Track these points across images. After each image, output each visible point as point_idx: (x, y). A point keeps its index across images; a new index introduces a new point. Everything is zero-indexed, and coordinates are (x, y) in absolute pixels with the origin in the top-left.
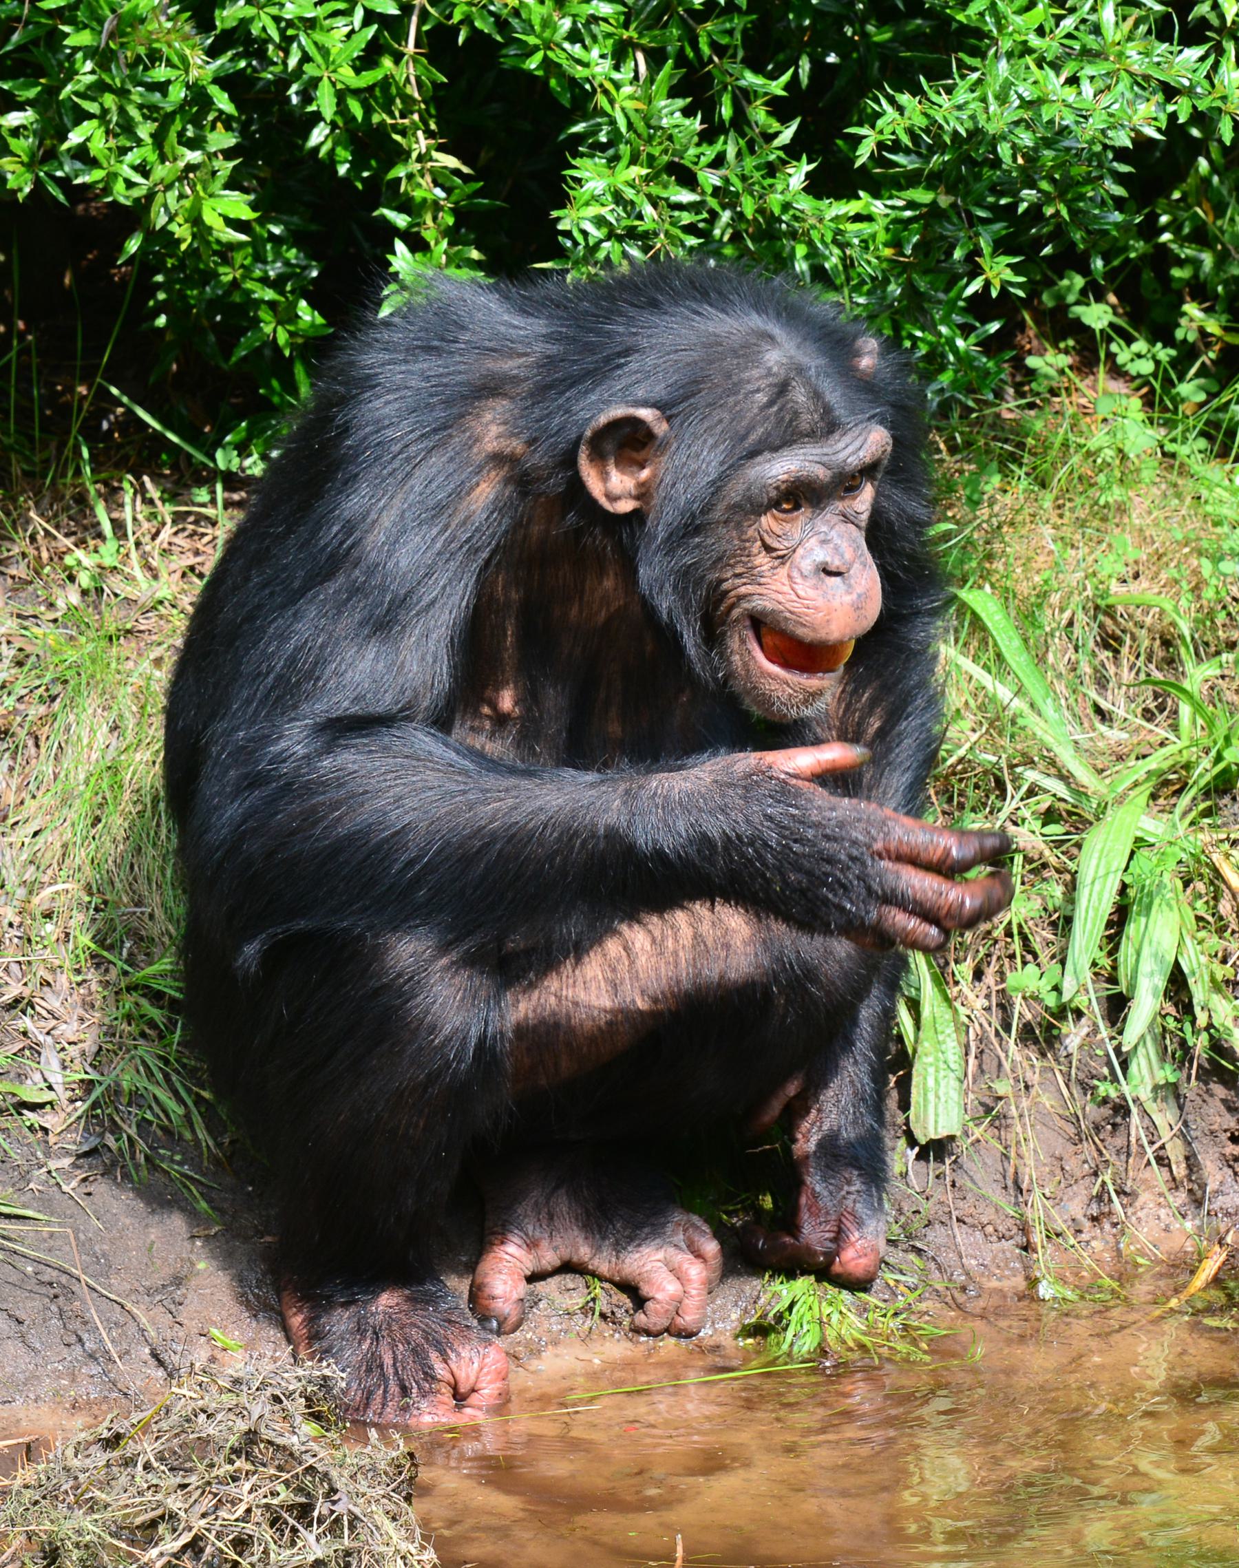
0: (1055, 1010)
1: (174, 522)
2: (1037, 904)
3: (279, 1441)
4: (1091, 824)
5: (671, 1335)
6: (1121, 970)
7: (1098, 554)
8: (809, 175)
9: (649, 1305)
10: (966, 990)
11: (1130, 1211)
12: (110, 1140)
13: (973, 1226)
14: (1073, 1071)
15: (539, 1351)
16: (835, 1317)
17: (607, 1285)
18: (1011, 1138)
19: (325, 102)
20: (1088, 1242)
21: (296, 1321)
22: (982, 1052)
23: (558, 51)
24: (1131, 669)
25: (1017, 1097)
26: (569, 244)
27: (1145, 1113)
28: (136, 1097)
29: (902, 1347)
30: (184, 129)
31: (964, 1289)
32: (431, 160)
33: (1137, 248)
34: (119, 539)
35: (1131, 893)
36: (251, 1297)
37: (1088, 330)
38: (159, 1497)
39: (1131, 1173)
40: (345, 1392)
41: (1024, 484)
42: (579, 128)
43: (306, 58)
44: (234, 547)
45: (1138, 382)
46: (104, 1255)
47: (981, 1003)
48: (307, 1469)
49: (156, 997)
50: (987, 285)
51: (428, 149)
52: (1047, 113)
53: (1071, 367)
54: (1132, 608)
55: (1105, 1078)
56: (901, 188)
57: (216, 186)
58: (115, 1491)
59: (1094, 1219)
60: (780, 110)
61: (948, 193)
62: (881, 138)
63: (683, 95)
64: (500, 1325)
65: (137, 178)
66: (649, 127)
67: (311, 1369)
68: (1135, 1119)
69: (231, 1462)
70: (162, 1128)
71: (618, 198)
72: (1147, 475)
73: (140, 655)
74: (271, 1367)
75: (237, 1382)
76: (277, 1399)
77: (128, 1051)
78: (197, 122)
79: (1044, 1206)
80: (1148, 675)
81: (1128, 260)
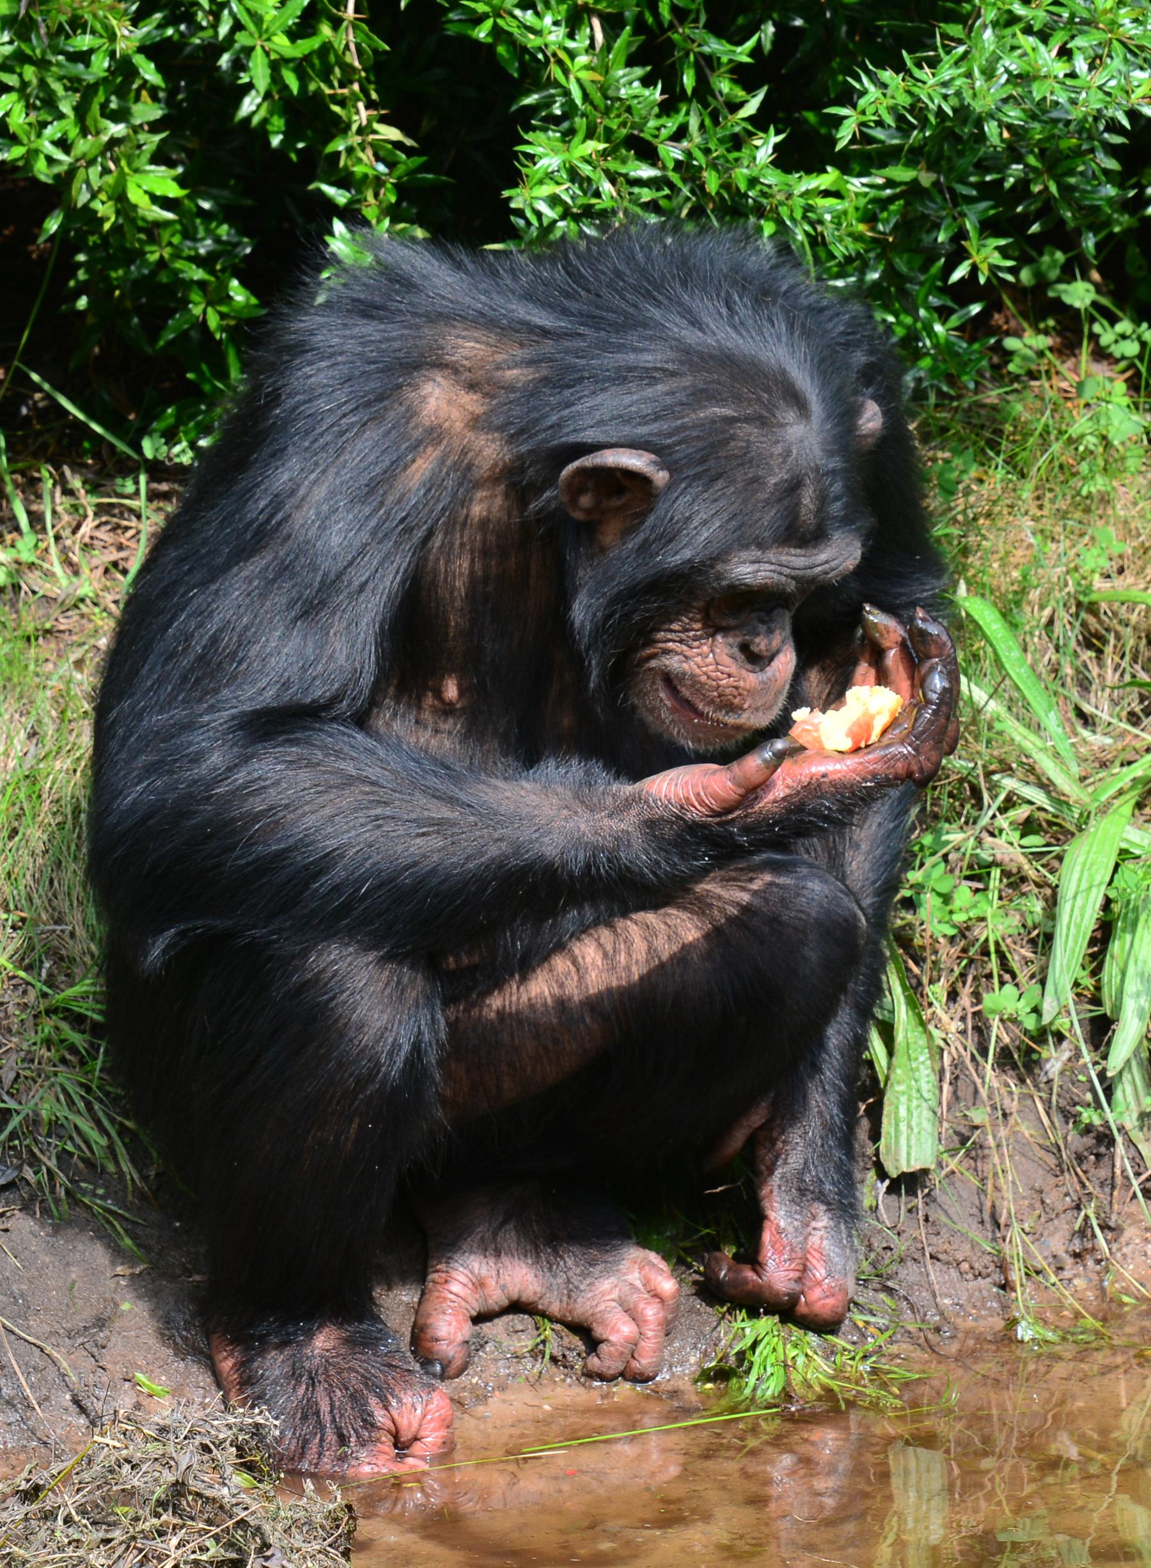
0: (1035, 1034)
1: (96, 514)
2: (1015, 920)
3: (208, 1493)
4: (1073, 834)
5: (625, 1379)
6: (1105, 990)
7: (1080, 547)
8: (777, 147)
9: (603, 1347)
10: (940, 1012)
11: (1115, 1247)
12: (28, 1173)
13: (948, 1263)
14: (1054, 1098)
15: (486, 1397)
16: (801, 1360)
17: (558, 1327)
18: (988, 1169)
19: (258, 73)
20: (1070, 1280)
21: (227, 1365)
22: (957, 1078)
23: (509, 19)
24: (1115, 670)
25: (994, 1125)
26: (521, 222)
27: (1130, 1143)
28: (56, 1127)
29: (871, 1391)
30: (108, 101)
31: (938, 1330)
32: (375, 132)
33: (1121, 223)
34: (37, 532)
35: (1116, 908)
36: (178, 1340)
37: (1069, 308)
38: (81, 1552)
39: (1116, 1207)
40: (279, 1441)
41: (1000, 473)
42: (531, 100)
43: (238, 26)
44: (162, 543)
45: (1123, 365)
46: (22, 1296)
47: (955, 1026)
48: (238, 1523)
49: (77, 1021)
50: (974, 269)
51: (369, 122)
52: (1038, 91)
53: (1051, 349)
54: (1116, 606)
55: (1089, 1105)
56: (883, 165)
57: (143, 161)
58: (34, 1547)
59: (1076, 1256)
60: (745, 77)
61: (929, 169)
62: (863, 118)
63: (643, 64)
64: (443, 1369)
65: (59, 155)
66: (606, 97)
67: (242, 1416)
68: (1120, 1149)
69: (158, 1515)
70: (84, 1160)
71: (574, 175)
72: (1132, 464)
73: (59, 656)
74: (200, 1414)
75: (163, 1430)
76: (206, 1449)
77: (48, 1078)
78: (122, 92)
79: (1023, 1242)
80: (1134, 676)
81: (1111, 235)
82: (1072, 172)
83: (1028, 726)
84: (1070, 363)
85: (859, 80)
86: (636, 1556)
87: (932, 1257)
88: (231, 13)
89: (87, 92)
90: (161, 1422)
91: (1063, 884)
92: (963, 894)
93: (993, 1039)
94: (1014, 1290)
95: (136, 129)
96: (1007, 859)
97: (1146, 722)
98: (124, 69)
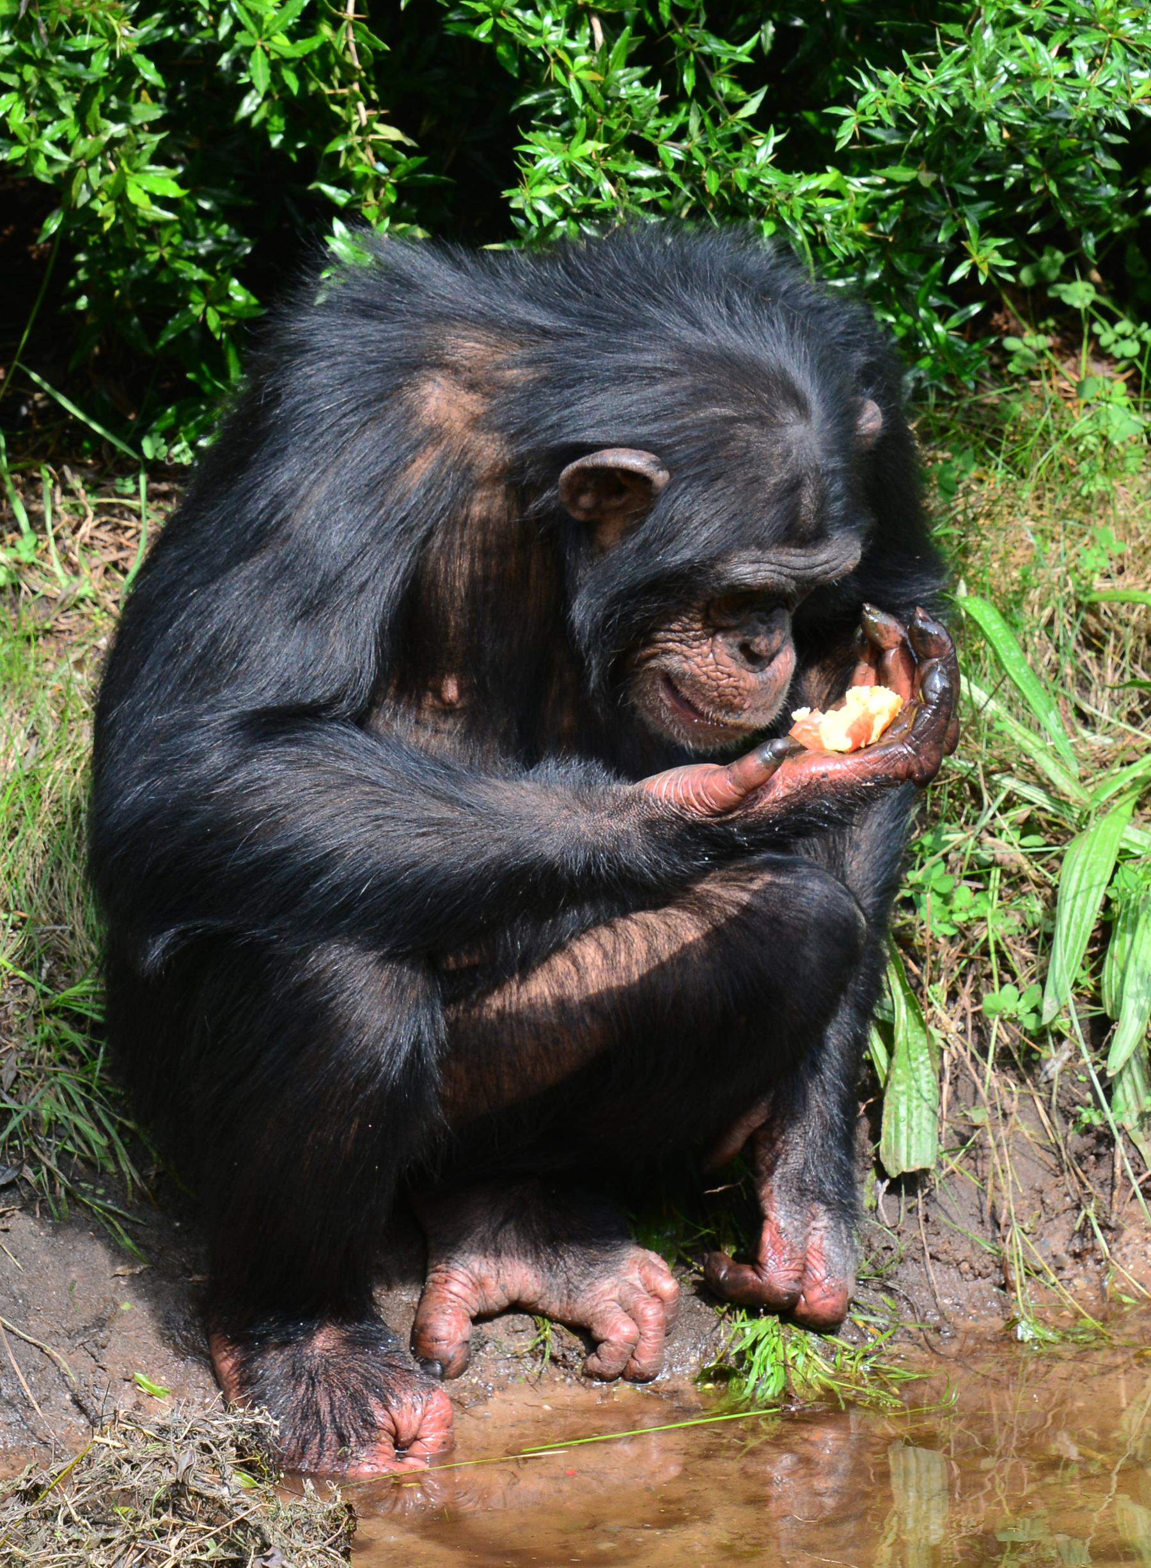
0: (1035, 1034)
1: (96, 514)
2: (1015, 920)
3: (208, 1493)
4: (1073, 834)
5: (625, 1379)
6: (1105, 990)
7: (1080, 547)
8: (777, 147)
9: (603, 1347)
10: (940, 1012)
11: (1115, 1247)
12: (28, 1173)
13: (948, 1263)
14: (1054, 1098)
15: (486, 1397)
16: (801, 1360)
17: (558, 1327)
18: (988, 1169)
19: (258, 73)
20: (1070, 1280)
21: (227, 1365)
22: (957, 1078)
23: (509, 19)
24: (1115, 670)
25: (994, 1125)
26: (521, 222)
27: (1130, 1143)
28: (56, 1127)
29: (871, 1391)
30: (108, 101)
31: (938, 1330)
32: (375, 132)
33: (1121, 223)
34: (37, 532)
35: (1116, 908)
36: (178, 1340)
37: (1069, 308)
38: (81, 1552)
39: (1116, 1207)
40: (279, 1441)
41: (1000, 473)
42: (531, 100)
43: (238, 26)
44: (162, 543)
45: (1123, 365)
46: (22, 1296)
47: (955, 1026)
48: (238, 1523)
49: (77, 1021)
50: (974, 269)
51: (369, 122)
52: (1038, 91)
53: (1051, 349)
54: (1116, 606)
55: (1089, 1105)
56: (883, 165)
57: (143, 161)
58: (34, 1547)
59: (1076, 1256)
60: (745, 77)
61: (929, 169)
62: (863, 118)
63: (643, 64)
64: (443, 1369)
65: (59, 155)
66: (606, 97)
67: (242, 1416)
68: (1120, 1149)
69: (158, 1515)
70: (84, 1160)
71: (574, 175)
72: (1132, 464)
73: (59, 656)
74: (200, 1414)
75: (163, 1430)
76: (206, 1449)
77: (48, 1078)
78: (122, 92)
79: (1023, 1242)
80: (1134, 676)
81: (1111, 235)
82: (1072, 172)
83: (1028, 726)
84: (1070, 363)
85: (859, 80)
86: (636, 1556)
87: (932, 1257)
88: (231, 13)
89: (87, 92)
90: (161, 1422)
91: (1063, 884)
92: (963, 894)
93: (993, 1039)
94: (1014, 1290)
95: (136, 129)
96: (1007, 859)
97: (1146, 722)
98: (124, 69)
